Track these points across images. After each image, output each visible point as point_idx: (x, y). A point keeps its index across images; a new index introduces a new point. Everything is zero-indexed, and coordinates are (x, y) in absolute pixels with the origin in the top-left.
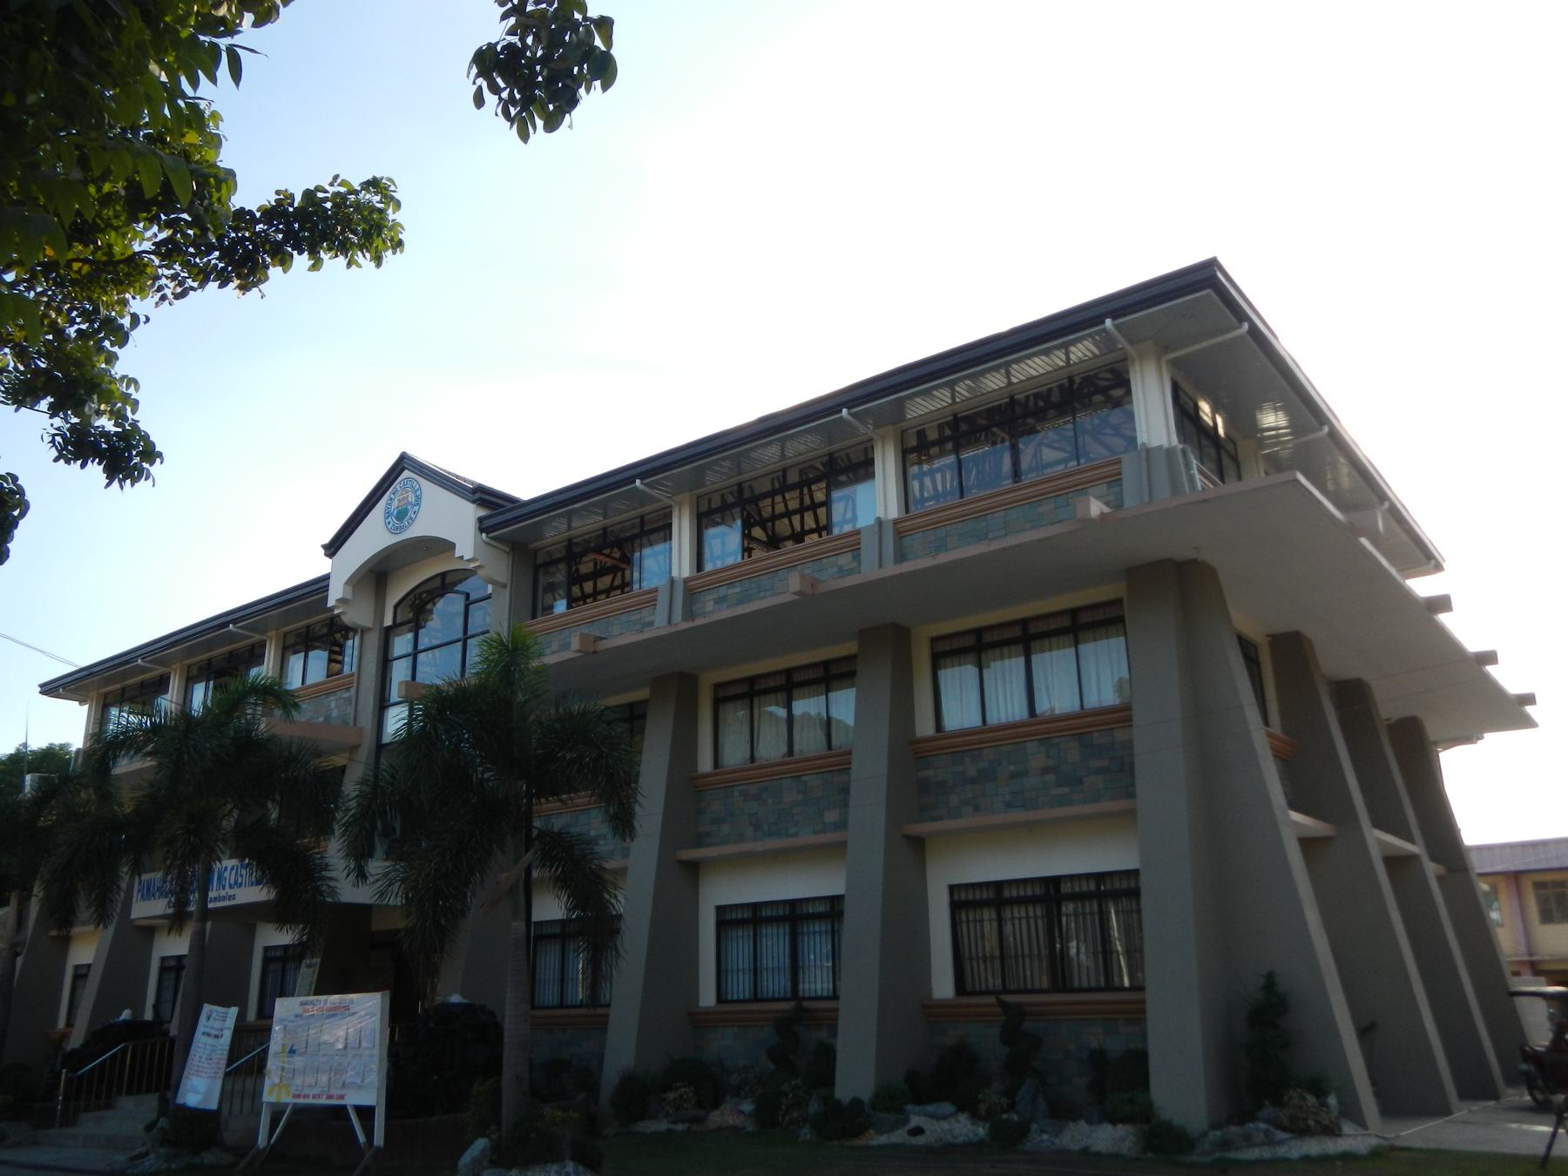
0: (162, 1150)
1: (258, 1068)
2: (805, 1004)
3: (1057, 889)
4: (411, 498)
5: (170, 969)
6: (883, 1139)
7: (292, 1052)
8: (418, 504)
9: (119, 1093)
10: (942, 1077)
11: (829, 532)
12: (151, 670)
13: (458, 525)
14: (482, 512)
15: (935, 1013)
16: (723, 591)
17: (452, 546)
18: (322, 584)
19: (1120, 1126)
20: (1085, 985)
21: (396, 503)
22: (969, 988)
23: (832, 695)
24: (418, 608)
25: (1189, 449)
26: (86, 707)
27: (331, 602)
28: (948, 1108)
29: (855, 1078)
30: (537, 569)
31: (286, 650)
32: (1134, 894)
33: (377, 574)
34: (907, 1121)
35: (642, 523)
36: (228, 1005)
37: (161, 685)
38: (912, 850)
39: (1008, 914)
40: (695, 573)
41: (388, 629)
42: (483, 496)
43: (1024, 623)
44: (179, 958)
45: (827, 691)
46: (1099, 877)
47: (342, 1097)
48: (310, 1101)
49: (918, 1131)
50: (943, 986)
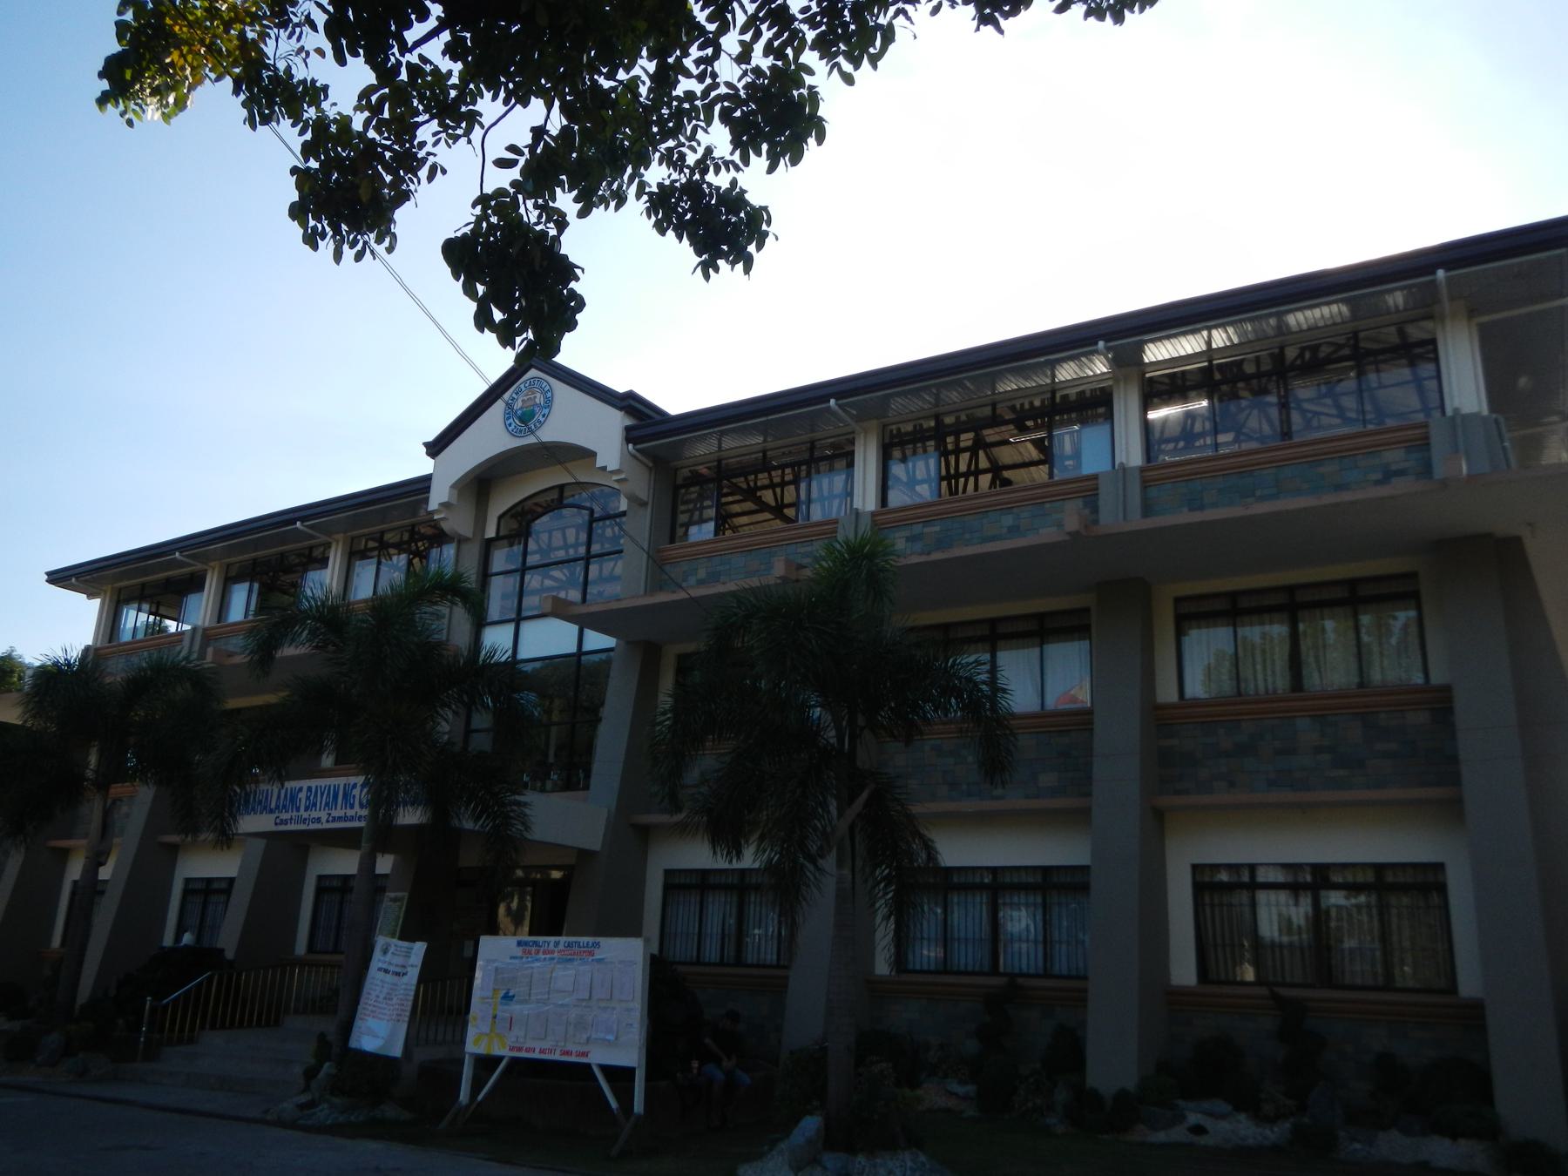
0: (336, 1100)
1: (460, 1011)
2: (1020, 980)
3: (1253, 875)
4: (539, 399)
5: (195, 892)
6: (1161, 1137)
7: (507, 997)
8: (550, 407)
9: (202, 1027)
10: (1200, 1065)
11: (1290, 438)
12: (313, 537)
13: (604, 435)
14: (629, 422)
15: (1177, 998)
16: (917, 529)
17: (592, 455)
18: (421, 485)
19: (1462, 1142)
20: (1065, 972)
22: (1002, 969)
24: (521, 522)
25: (1501, 419)
26: (97, 602)
27: (433, 505)
28: (1222, 1106)
29: (1113, 1064)
30: (676, 488)
31: (355, 554)
32: (1084, 888)
33: (481, 483)
34: (1183, 1118)
35: (812, 448)
36: (413, 940)
37: (195, 583)
38: (1157, 821)
39: (1207, 899)
40: (936, 499)
41: (490, 541)
42: (631, 404)
43: (1291, 589)
44: (346, 878)
45: (1041, 645)
46: (1046, 870)
47: (585, 1054)
48: (536, 1055)
49: (1199, 1130)
50: (1184, 971)
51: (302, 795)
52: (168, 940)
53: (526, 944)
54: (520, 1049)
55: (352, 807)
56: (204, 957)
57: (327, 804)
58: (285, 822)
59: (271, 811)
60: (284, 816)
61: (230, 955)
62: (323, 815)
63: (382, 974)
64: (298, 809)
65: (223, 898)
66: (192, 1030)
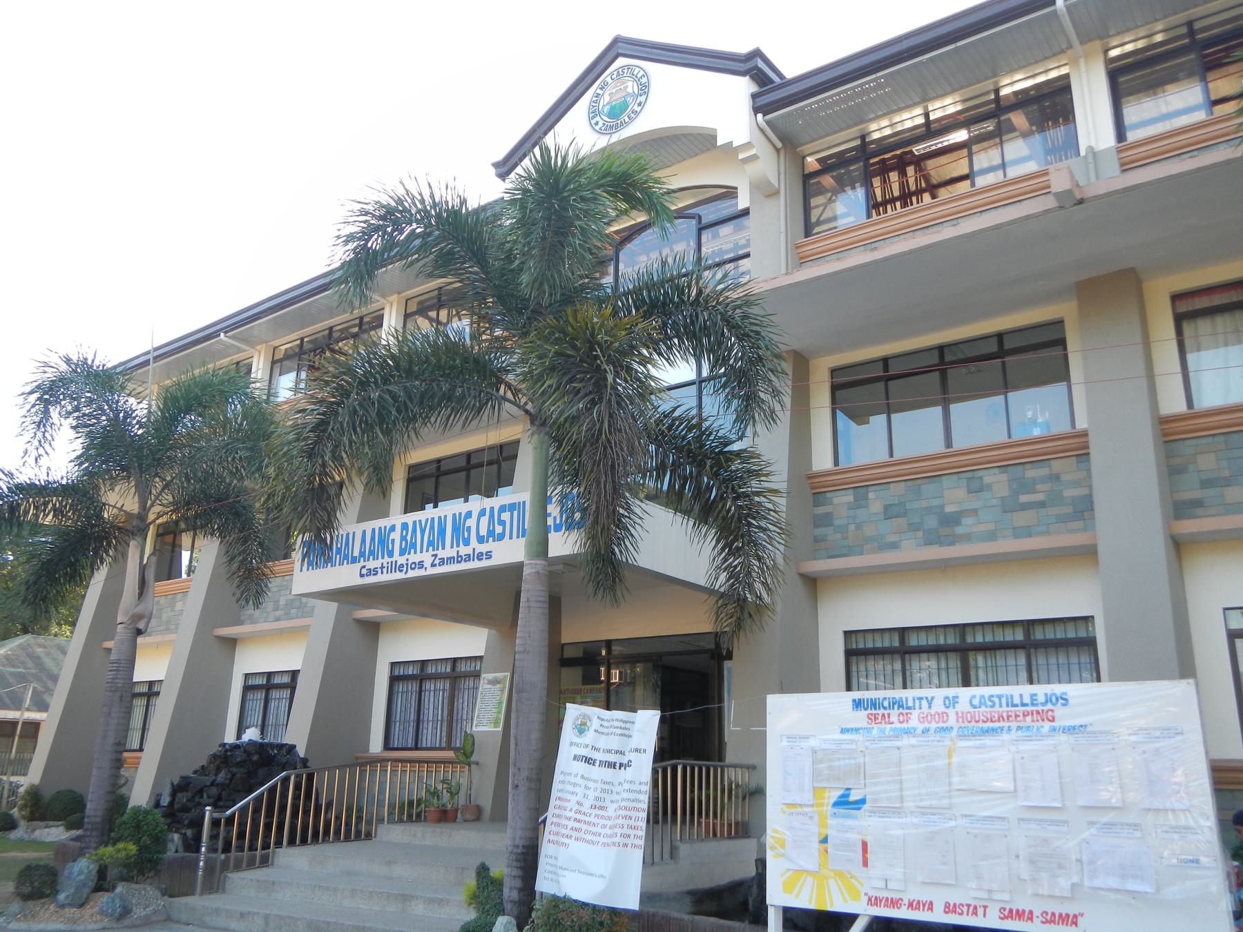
4: (632, 87)
8: (647, 94)
9: (279, 843)
21: (607, 98)
23: (1009, 395)
30: (807, 177)
45: (946, 404)
51: (396, 536)
52: (230, 738)
53: (874, 704)
54: (894, 903)
55: (467, 543)
56: (265, 759)
57: (430, 543)
58: (374, 572)
59: (354, 560)
60: (372, 564)
61: (301, 751)
62: (427, 558)
63: (581, 767)
64: (391, 554)
65: (286, 693)
66: (266, 846)
